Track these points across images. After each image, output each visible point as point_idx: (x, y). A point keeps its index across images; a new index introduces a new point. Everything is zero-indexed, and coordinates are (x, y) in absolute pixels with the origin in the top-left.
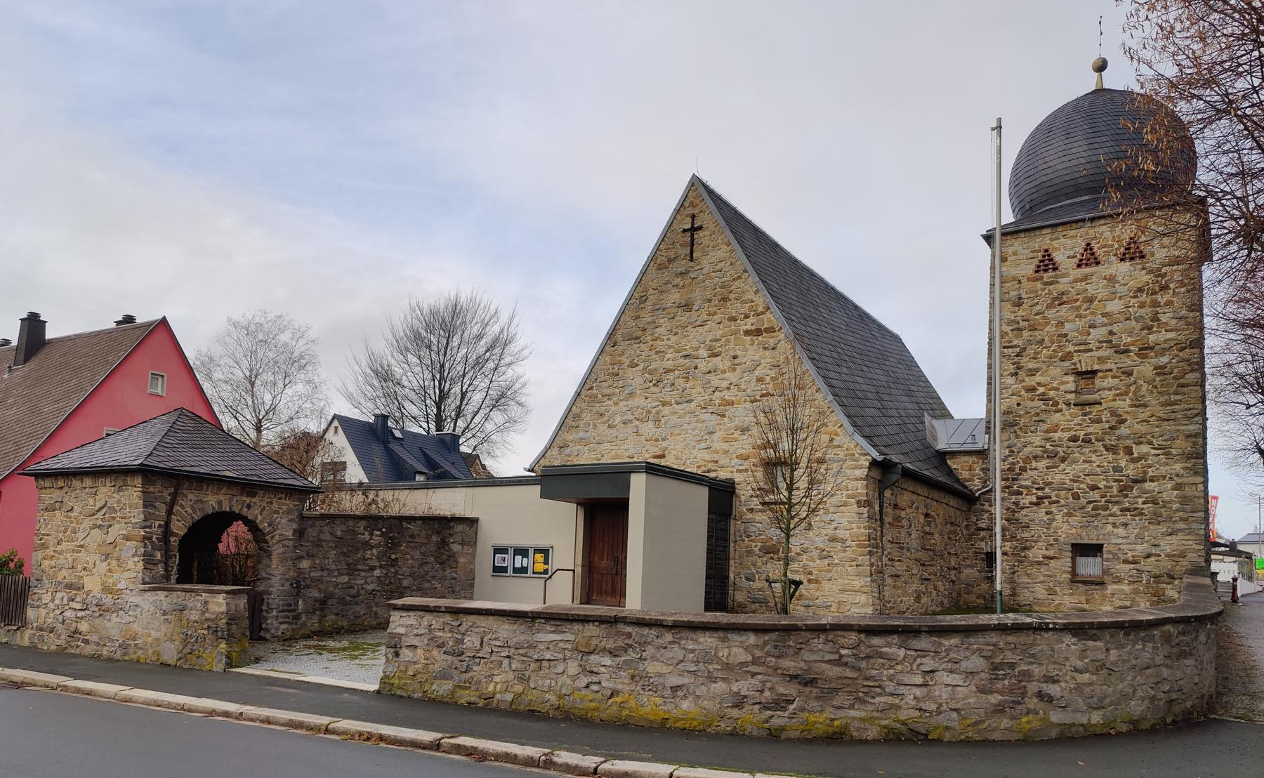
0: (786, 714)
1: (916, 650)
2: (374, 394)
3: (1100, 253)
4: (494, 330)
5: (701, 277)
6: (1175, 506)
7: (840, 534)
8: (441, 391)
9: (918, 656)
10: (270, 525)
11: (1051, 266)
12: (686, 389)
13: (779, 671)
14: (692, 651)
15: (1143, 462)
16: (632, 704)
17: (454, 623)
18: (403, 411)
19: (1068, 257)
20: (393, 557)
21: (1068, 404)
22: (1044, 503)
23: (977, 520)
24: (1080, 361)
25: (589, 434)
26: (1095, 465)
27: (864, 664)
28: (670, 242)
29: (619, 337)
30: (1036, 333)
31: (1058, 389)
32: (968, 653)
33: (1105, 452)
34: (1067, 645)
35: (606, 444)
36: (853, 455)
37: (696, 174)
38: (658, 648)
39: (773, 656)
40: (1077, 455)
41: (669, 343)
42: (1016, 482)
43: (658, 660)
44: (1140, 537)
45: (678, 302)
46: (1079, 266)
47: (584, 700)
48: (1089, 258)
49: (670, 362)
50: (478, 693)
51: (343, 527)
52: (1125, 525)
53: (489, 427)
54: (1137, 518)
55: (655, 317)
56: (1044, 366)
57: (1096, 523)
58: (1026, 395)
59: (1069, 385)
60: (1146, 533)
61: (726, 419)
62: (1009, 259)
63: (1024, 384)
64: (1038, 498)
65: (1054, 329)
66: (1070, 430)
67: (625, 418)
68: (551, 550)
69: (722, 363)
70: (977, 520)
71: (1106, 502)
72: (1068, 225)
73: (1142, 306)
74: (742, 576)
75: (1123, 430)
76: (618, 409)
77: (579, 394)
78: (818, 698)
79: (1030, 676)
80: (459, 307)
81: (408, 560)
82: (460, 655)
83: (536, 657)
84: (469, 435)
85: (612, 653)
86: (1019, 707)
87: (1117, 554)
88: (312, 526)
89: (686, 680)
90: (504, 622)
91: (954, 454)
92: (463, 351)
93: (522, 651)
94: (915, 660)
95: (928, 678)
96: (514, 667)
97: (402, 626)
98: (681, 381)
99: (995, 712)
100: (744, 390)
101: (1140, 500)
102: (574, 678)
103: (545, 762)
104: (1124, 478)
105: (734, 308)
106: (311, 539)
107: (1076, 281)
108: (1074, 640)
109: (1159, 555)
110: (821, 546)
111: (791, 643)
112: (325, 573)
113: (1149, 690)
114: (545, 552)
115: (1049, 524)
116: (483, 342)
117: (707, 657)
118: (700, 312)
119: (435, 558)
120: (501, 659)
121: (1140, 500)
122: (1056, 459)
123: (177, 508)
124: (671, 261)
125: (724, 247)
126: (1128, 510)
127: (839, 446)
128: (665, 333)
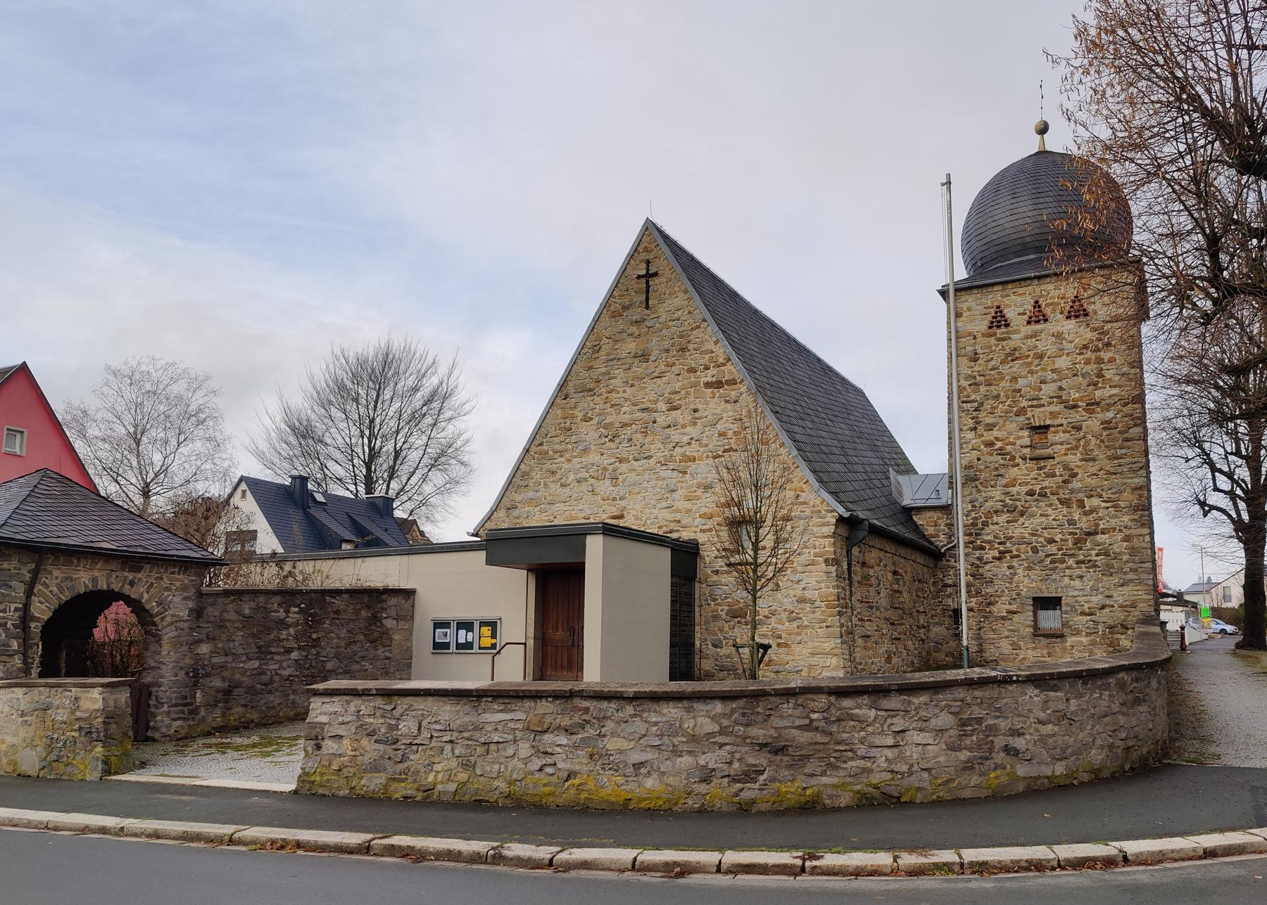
0: (757, 786)
1: (886, 710)
2: (291, 453)
3: (1048, 311)
4: (431, 383)
5: (658, 325)
6: (1125, 558)
7: (808, 594)
8: (371, 449)
9: (889, 716)
10: (159, 604)
11: (1003, 323)
12: (644, 444)
13: (748, 741)
14: (656, 724)
15: (1094, 515)
16: (591, 785)
17: (389, 707)
18: (327, 471)
19: (1019, 314)
20: (314, 636)
21: (1024, 459)
22: (1005, 557)
23: (944, 577)
24: (1033, 416)
25: (539, 494)
26: (1051, 518)
27: (834, 728)
28: (625, 288)
29: (570, 388)
30: (992, 388)
31: (1014, 444)
32: (937, 711)
33: (1060, 506)
34: (1031, 697)
35: (558, 505)
36: (820, 511)
37: (650, 218)
38: (618, 723)
39: (741, 725)
40: (1034, 509)
41: (625, 395)
42: (979, 537)
43: (619, 736)
44: (1094, 589)
45: (633, 352)
46: (1029, 323)
47: (538, 785)
48: (1038, 316)
49: (627, 416)
50: (415, 786)
51: (253, 604)
52: (1081, 577)
53: (428, 488)
54: (1091, 570)
55: (609, 368)
56: (1001, 422)
57: (1054, 576)
58: (985, 449)
59: (1024, 440)
60: (1100, 585)
61: (688, 476)
62: (964, 314)
63: (983, 438)
64: (1000, 553)
65: (1008, 384)
66: (1027, 484)
67: (579, 476)
68: (499, 622)
69: (681, 416)
70: (944, 577)
71: (1062, 554)
72: (1017, 283)
73: (1087, 362)
74: (709, 642)
75: (1075, 484)
76: (571, 467)
77: (528, 451)
78: (789, 767)
79: (997, 730)
80: (391, 357)
81: (332, 639)
82: (395, 743)
83: (482, 740)
84: (405, 498)
85: (568, 731)
86: (987, 763)
87: (1074, 606)
88: (213, 604)
89: (649, 756)
90: (445, 703)
91: (919, 509)
92: (396, 405)
93: (466, 735)
94: (886, 721)
95: (899, 738)
96: (457, 752)
97: (325, 714)
98: (639, 436)
99: (965, 769)
100: (706, 446)
101: (1094, 553)
102: (526, 761)
103: (493, 857)
104: (1078, 531)
105: (694, 359)
106: (212, 619)
107: (1027, 337)
108: (1036, 691)
109: (1113, 606)
110: (790, 607)
111: (760, 710)
112: (230, 659)
113: (1108, 738)
114: (493, 625)
115: (1012, 579)
116: (419, 395)
117: (672, 729)
118: (657, 363)
119: (365, 635)
120: (442, 744)
121: (1094, 553)
122: (1016, 514)
123: (38, 588)
124: (625, 308)
125: (681, 295)
126: (1083, 562)
127: (805, 503)
128: (621, 384)
